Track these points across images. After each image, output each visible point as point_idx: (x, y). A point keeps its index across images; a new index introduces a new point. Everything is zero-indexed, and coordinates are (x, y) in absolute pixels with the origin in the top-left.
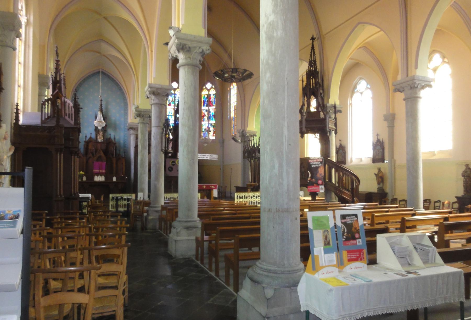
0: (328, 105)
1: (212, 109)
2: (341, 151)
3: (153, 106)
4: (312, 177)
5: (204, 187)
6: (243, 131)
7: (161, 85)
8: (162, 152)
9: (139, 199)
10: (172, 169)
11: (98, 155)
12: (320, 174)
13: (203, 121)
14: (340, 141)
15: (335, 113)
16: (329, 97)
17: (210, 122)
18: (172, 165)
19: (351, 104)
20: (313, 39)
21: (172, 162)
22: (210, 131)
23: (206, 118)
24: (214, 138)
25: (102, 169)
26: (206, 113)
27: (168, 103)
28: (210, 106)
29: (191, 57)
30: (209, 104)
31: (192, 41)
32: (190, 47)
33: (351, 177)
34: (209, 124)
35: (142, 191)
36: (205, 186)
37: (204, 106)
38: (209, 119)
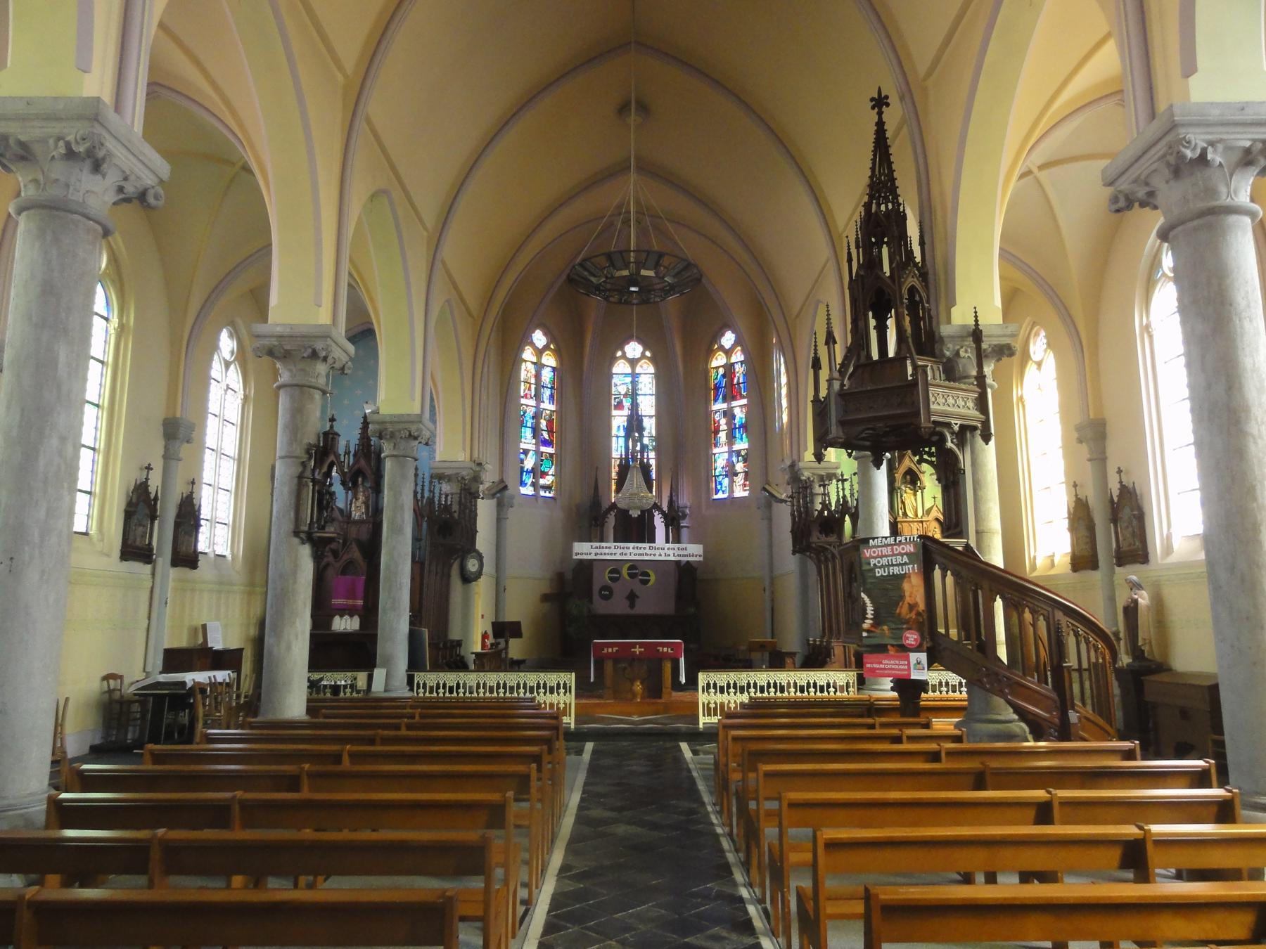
0: (945, 330)
1: (739, 409)
2: (1126, 513)
3: (282, 392)
4: (878, 621)
5: (637, 650)
6: (793, 466)
7: (291, 326)
8: (296, 540)
9: (374, 688)
10: (611, 593)
11: (346, 557)
12: (912, 607)
13: (716, 446)
14: (1120, 471)
15: (980, 357)
16: (951, 302)
17: (736, 447)
18: (611, 579)
19: (1147, 328)
20: (880, 102)
21: (611, 572)
22: (736, 474)
23: (722, 436)
24: (746, 494)
25: (354, 598)
26: (723, 421)
27: (613, 403)
28: (734, 398)
29: (41, 178)
30: (731, 395)
31: (22, 119)
32: (22, 144)
33: (1047, 619)
34: (731, 452)
35: (388, 663)
36: (641, 645)
37: (716, 400)
38: (731, 438)
